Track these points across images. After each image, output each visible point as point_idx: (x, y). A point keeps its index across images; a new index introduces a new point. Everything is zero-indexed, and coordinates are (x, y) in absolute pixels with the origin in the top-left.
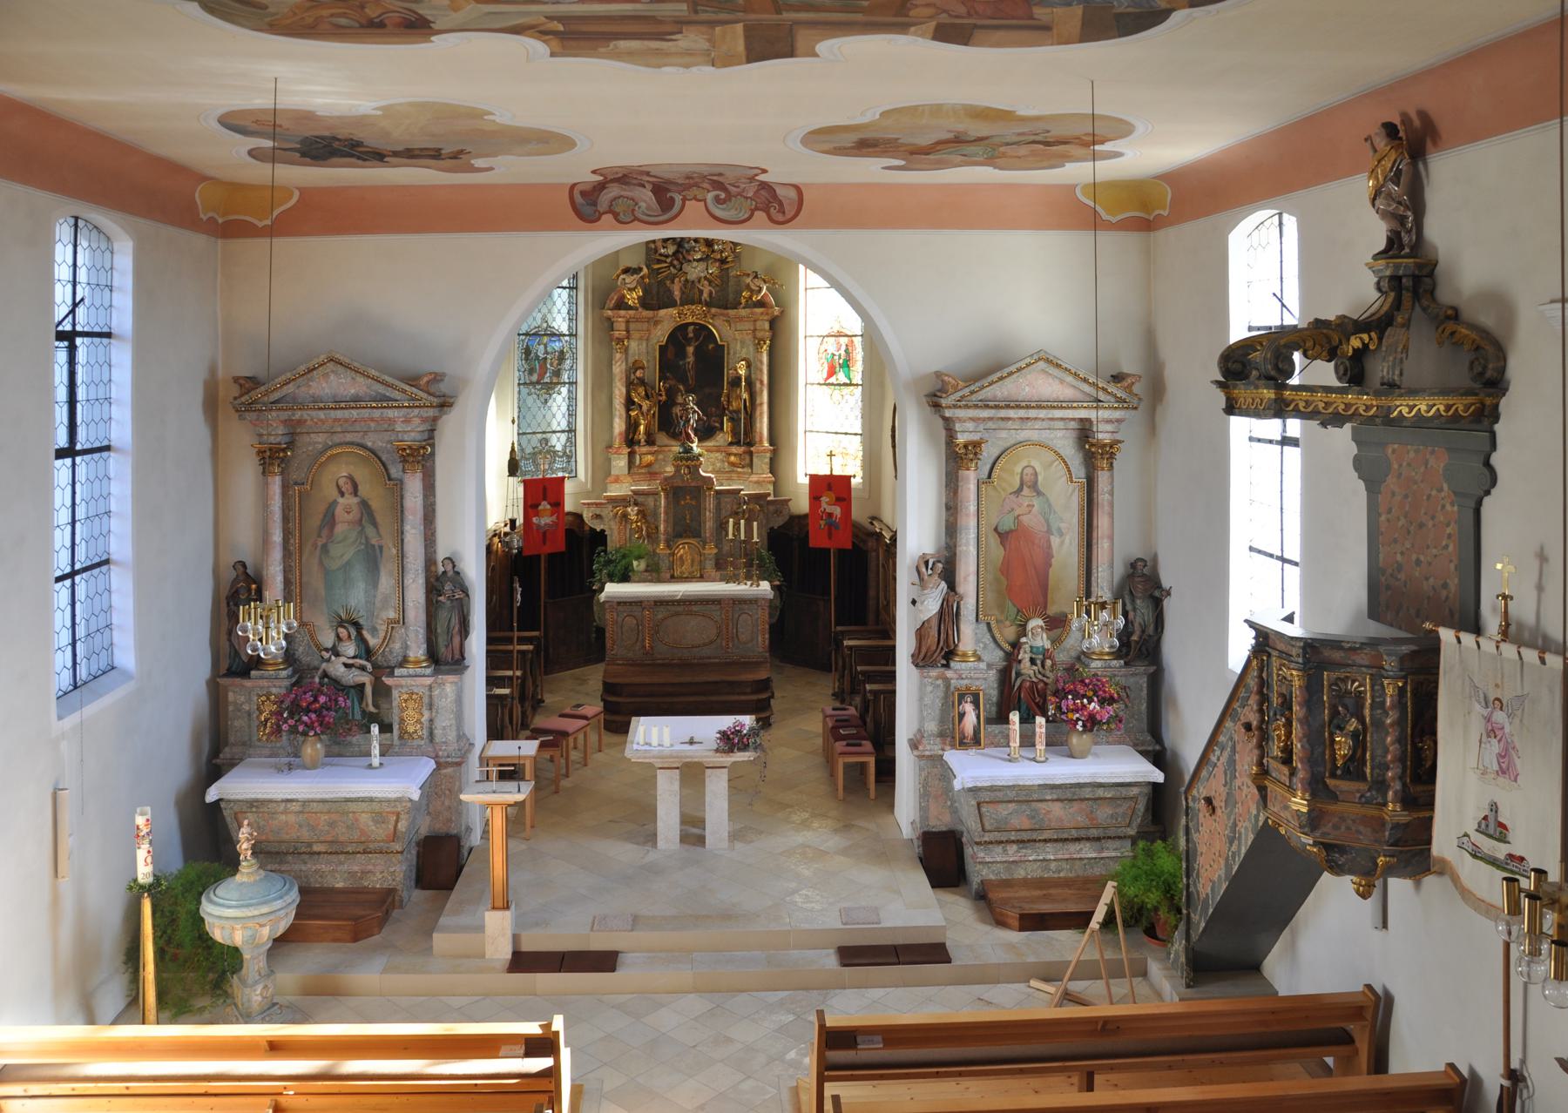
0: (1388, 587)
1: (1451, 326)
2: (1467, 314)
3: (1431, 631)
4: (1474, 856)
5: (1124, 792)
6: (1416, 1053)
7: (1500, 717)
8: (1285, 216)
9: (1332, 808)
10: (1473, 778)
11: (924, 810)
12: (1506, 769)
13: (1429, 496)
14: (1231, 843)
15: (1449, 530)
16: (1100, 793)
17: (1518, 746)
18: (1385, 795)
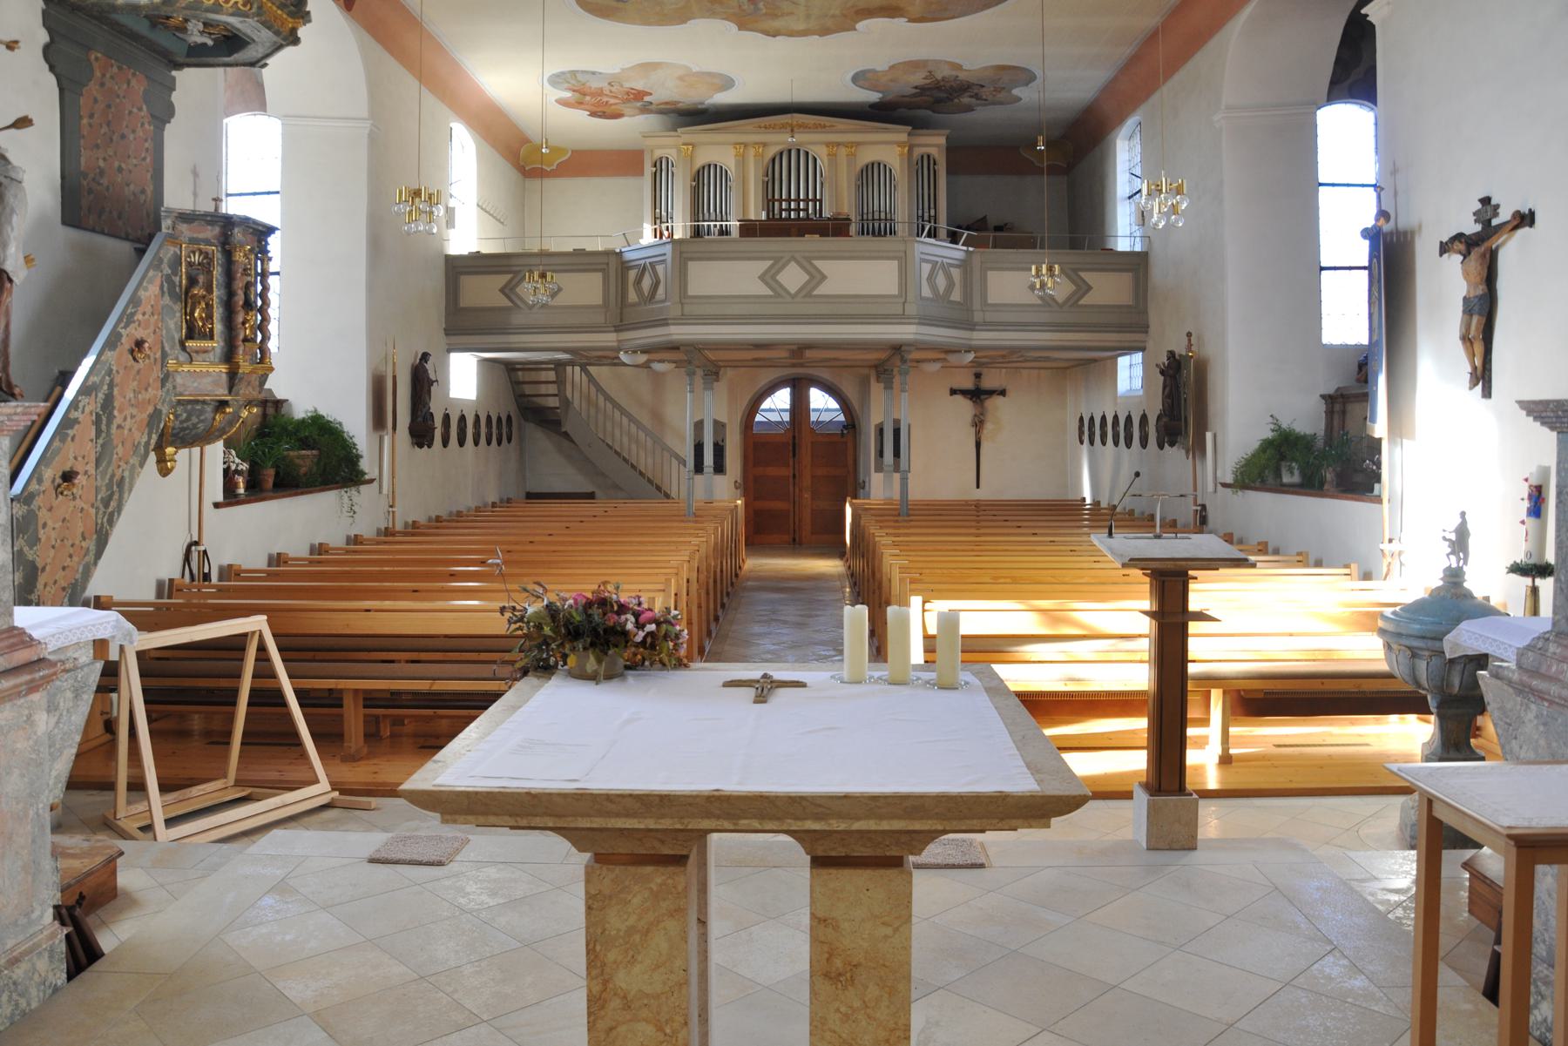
0: (90, 191)
11: (1381, 511)
14: (107, 505)
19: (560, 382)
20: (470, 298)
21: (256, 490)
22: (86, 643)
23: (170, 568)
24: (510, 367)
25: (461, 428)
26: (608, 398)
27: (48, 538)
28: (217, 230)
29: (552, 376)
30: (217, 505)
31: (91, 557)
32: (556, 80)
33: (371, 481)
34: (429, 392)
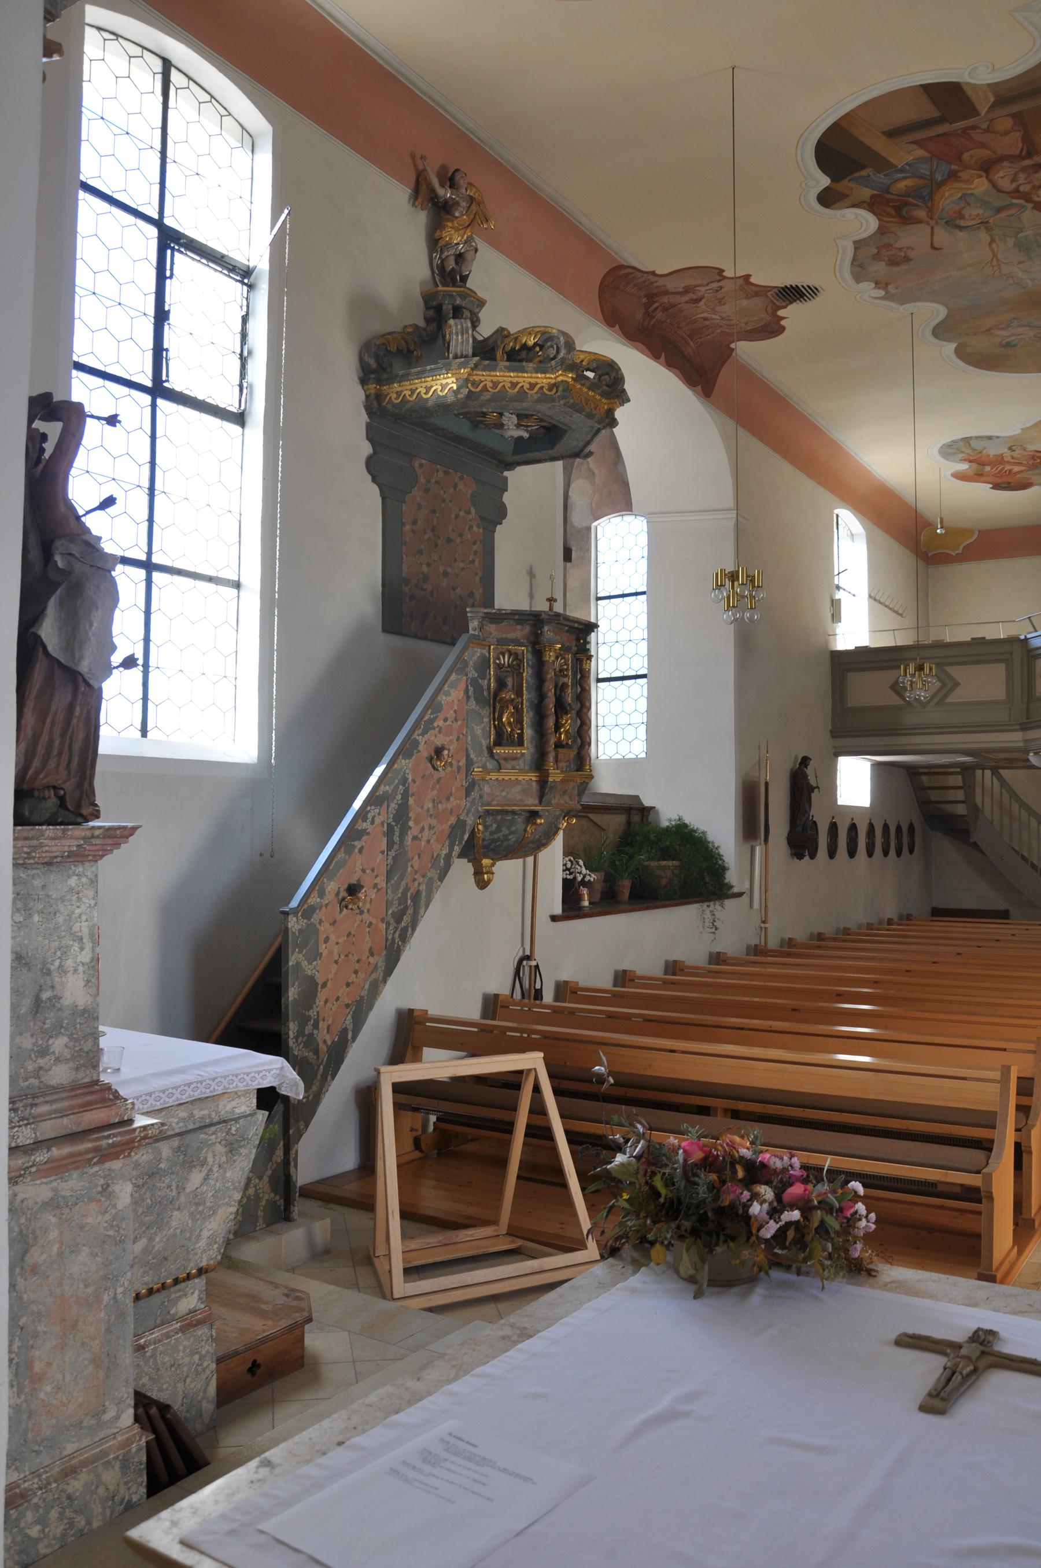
0: (412, 597)
13: (457, 516)
14: (398, 921)
15: (475, 548)
19: (969, 787)
20: (856, 698)
21: (608, 902)
22: (247, 1092)
23: (499, 981)
24: (911, 771)
25: (852, 835)
26: (1023, 805)
27: (331, 953)
28: (527, 629)
29: (958, 780)
30: (554, 918)
31: (380, 974)
32: (949, 451)
33: (740, 895)
34: (809, 798)
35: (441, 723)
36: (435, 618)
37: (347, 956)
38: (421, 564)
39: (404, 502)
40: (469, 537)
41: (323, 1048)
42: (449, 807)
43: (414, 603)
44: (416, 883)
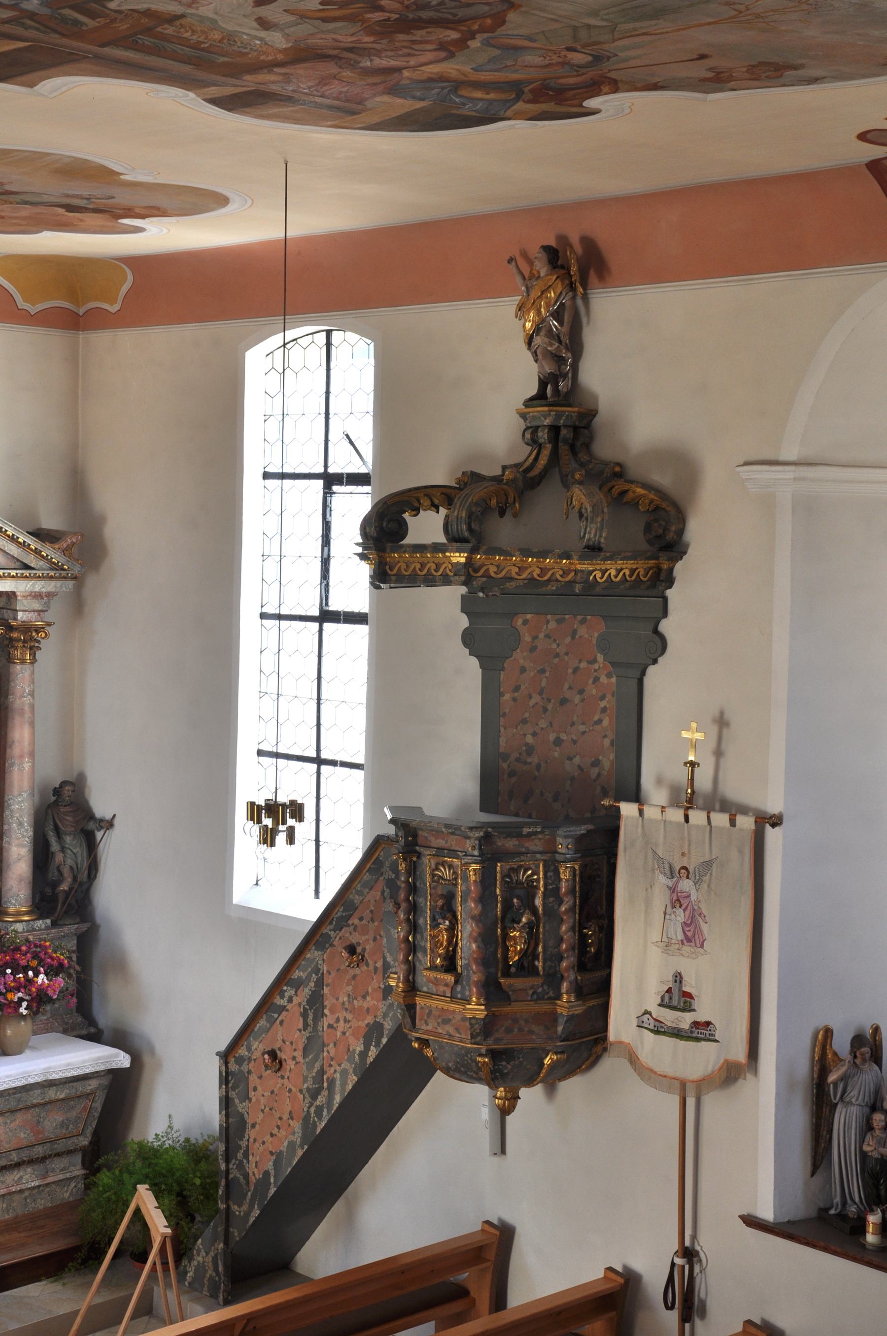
0: (512, 774)
1: (619, 486)
2: (634, 471)
3: (611, 806)
4: (657, 1032)
5: (80, 1087)
6: (543, 1275)
7: (686, 885)
8: (336, 337)
9: (507, 1009)
10: (655, 955)
12: (692, 936)
13: (576, 670)
14: (314, 1097)
15: (603, 704)
16: (52, 1094)
17: (705, 912)
18: (559, 988)
35: (356, 921)
36: (542, 794)
37: (271, 1109)
38: (525, 735)
39: (503, 669)
40: (594, 692)
41: (253, 1180)
42: (366, 1005)
43: (514, 780)
44: (332, 1070)
